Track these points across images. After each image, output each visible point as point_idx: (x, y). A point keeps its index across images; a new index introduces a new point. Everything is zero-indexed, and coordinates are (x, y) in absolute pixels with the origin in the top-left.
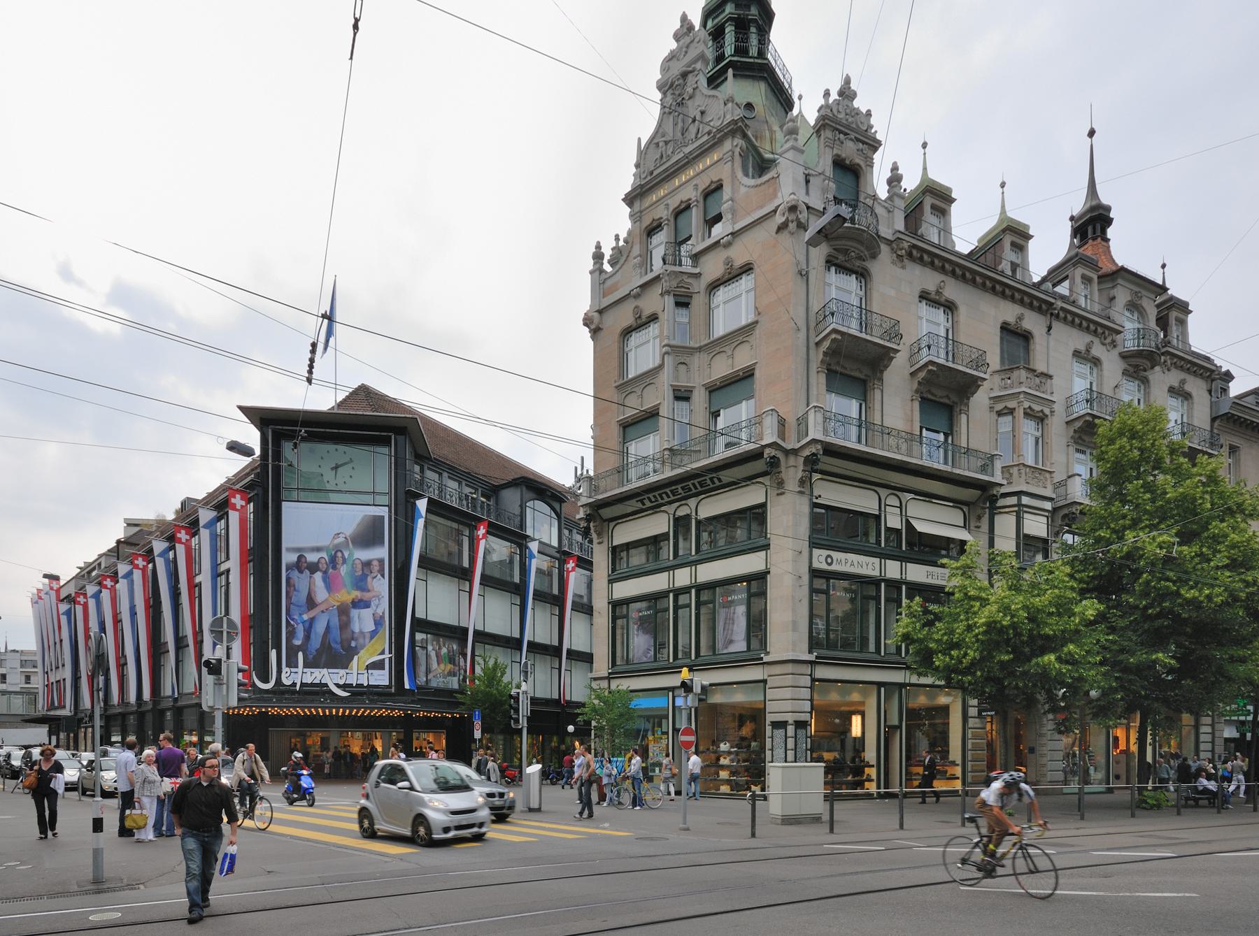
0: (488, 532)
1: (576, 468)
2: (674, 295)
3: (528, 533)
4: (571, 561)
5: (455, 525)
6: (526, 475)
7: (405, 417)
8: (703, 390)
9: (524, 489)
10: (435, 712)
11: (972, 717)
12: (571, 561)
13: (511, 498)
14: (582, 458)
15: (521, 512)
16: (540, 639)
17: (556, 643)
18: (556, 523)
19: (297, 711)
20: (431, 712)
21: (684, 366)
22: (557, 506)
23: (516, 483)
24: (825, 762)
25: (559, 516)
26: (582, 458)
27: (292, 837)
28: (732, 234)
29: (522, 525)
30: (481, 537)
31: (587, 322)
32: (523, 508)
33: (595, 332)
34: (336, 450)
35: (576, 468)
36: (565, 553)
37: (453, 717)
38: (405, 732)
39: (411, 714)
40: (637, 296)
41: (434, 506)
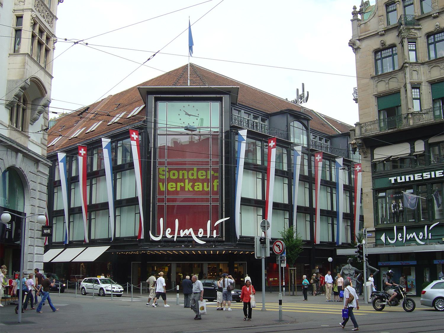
0: (277, 145)
1: (298, 90)
2: (407, 38)
3: (292, 141)
4: (272, 141)
5: (254, 141)
6: (290, 108)
7: (232, 88)
8: (427, 84)
9: (289, 116)
10: (128, 252)
11: (174, 187)
12: (272, 141)
13: (280, 122)
14: (303, 84)
15: (288, 129)
16: (251, 195)
17: (286, 202)
18: (305, 132)
19: (161, 252)
20: (131, 252)
21: (415, 72)
22: (305, 122)
23: (282, 113)
24: (420, 300)
25: (307, 128)
26: (303, 84)
27: (237, 309)
28: (438, 13)
29: (288, 137)
30: (318, 160)
31: (352, 44)
32: (288, 126)
33: (356, 50)
34: (189, 105)
35: (298, 90)
36: (312, 150)
37: (121, 254)
38: (336, 254)
39: (118, 254)
40: (382, 35)
41: (250, 134)
